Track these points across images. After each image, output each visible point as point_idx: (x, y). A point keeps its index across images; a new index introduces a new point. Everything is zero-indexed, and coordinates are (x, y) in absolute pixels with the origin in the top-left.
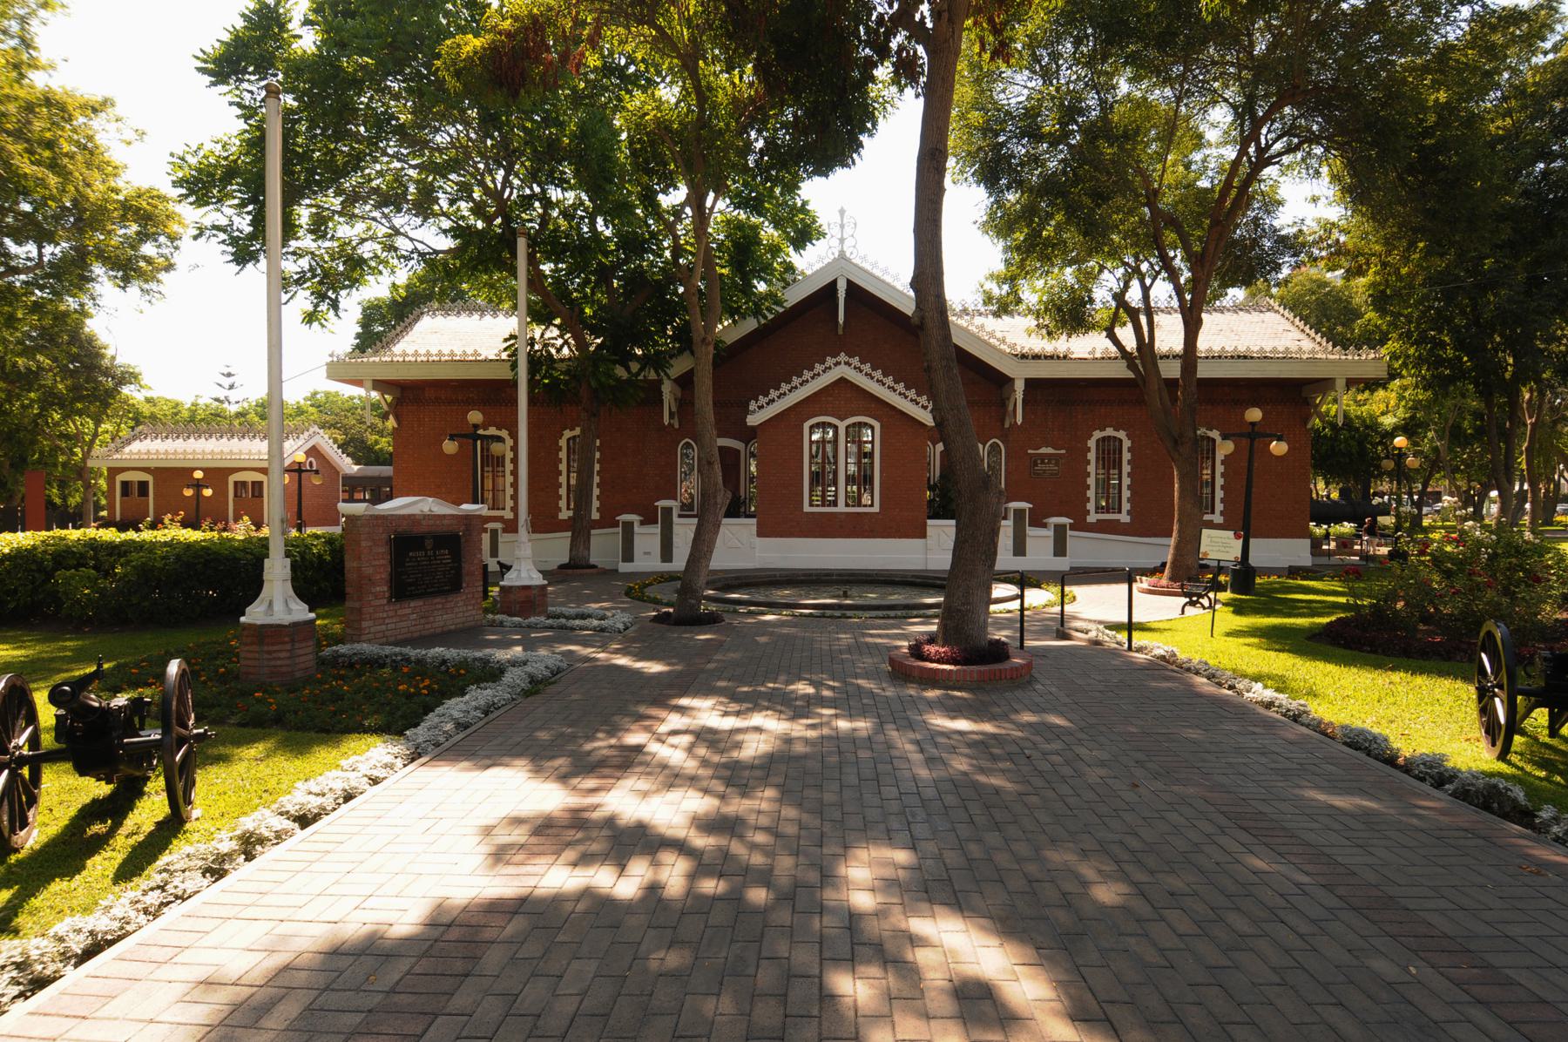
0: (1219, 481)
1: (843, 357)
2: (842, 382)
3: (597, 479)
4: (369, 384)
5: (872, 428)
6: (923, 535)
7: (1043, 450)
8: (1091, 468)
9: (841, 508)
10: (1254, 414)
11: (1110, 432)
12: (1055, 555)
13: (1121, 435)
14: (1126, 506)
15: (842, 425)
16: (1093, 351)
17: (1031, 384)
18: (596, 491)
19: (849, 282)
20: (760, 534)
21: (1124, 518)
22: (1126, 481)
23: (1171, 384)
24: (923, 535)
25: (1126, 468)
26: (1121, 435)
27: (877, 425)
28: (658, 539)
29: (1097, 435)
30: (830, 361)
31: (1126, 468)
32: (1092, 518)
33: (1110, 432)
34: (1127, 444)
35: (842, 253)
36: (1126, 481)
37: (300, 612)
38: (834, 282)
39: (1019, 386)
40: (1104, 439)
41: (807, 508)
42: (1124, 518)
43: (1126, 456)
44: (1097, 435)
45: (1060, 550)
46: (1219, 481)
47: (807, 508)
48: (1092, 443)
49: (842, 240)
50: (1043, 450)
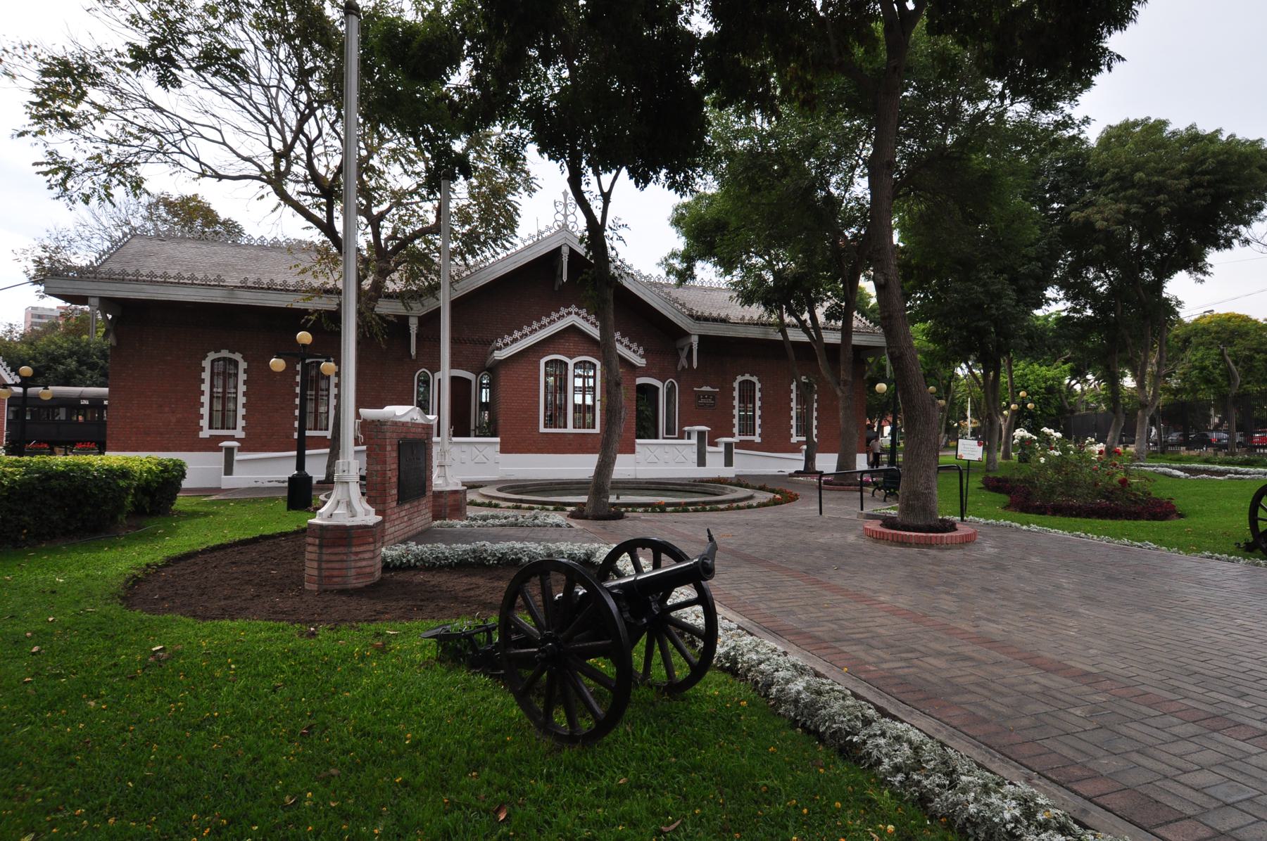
0: (205, 399)
1: (573, 309)
2: (572, 329)
3: (815, 414)
4: (95, 302)
5: (594, 366)
6: (633, 452)
7: (705, 389)
8: (793, 404)
9: (570, 429)
10: (304, 337)
11: (747, 377)
12: (726, 465)
13: (754, 379)
14: (758, 431)
15: (571, 363)
16: (743, 318)
17: (702, 338)
18: (815, 423)
19: (571, 249)
20: (503, 451)
21: (757, 439)
22: (758, 413)
23: (832, 348)
24: (633, 452)
25: (758, 404)
26: (754, 379)
27: (598, 364)
28: (695, 449)
29: (740, 378)
30: (563, 311)
31: (758, 404)
32: (205, 433)
33: (747, 377)
34: (758, 386)
35: (565, 226)
36: (758, 413)
37: (366, 515)
38: (559, 249)
39: (695, 340)
40: (552, 361)
41: (542, 429)
42: (757, 439)
43: (758, 395)
44: (740, 378)
45: (729, 462)
46: (205, 399)
47: (542, 429)
48: (736, 385)
49: (566, 216)
50: (705, 389)
